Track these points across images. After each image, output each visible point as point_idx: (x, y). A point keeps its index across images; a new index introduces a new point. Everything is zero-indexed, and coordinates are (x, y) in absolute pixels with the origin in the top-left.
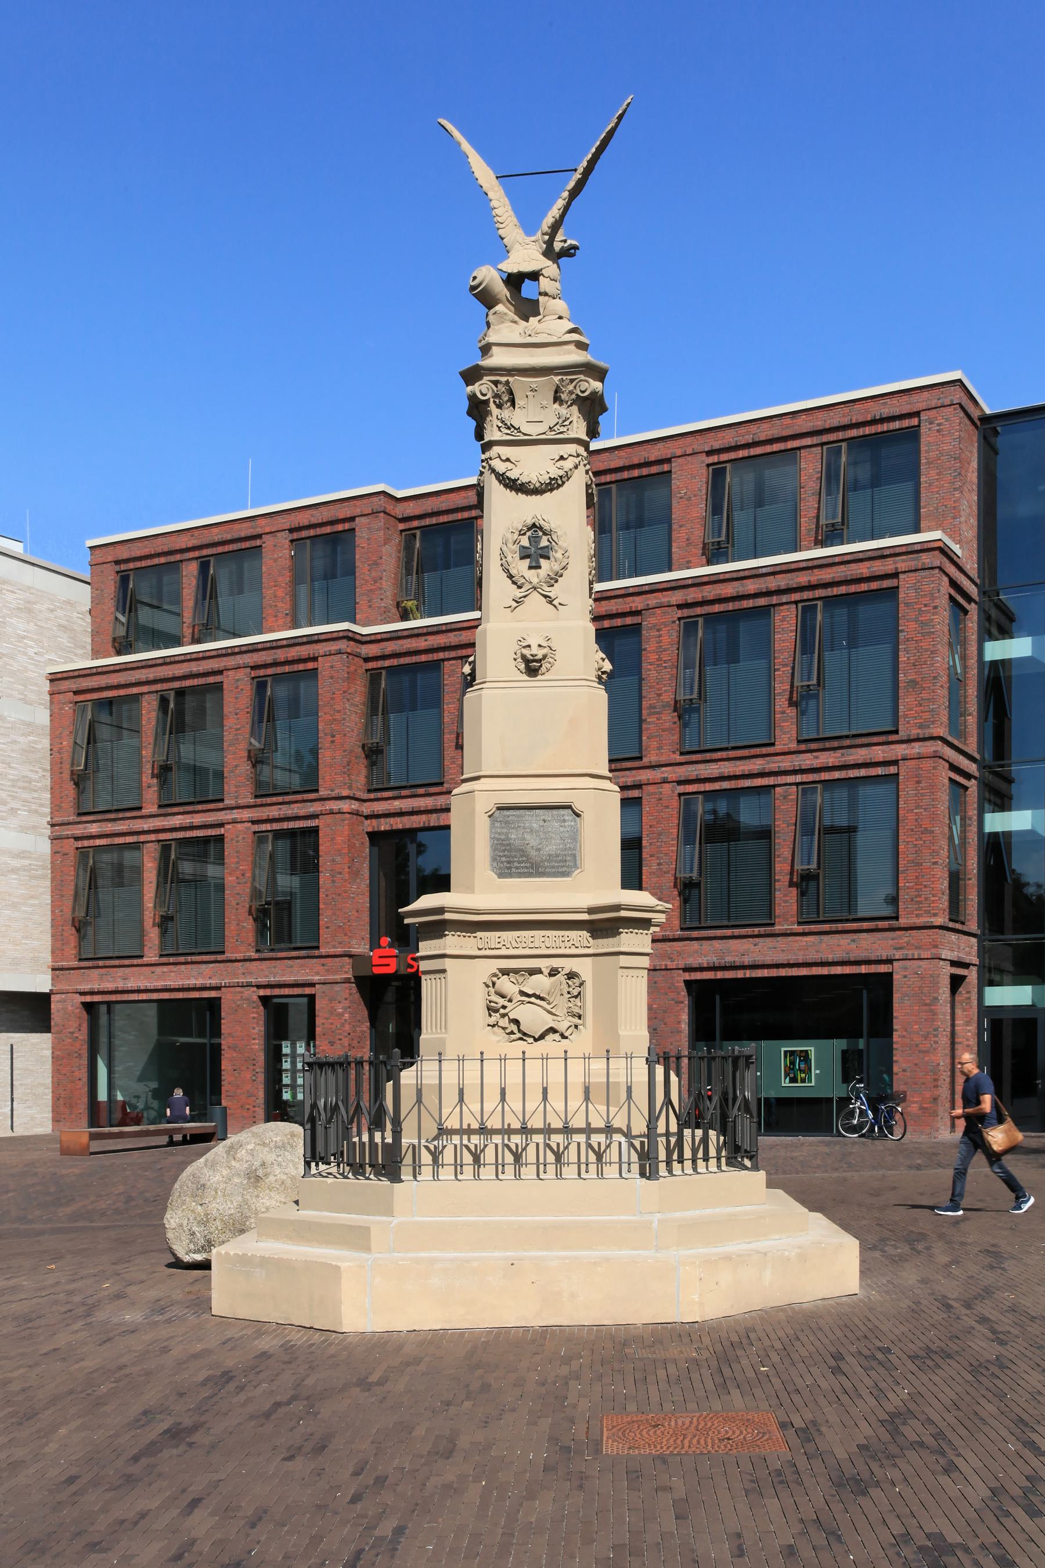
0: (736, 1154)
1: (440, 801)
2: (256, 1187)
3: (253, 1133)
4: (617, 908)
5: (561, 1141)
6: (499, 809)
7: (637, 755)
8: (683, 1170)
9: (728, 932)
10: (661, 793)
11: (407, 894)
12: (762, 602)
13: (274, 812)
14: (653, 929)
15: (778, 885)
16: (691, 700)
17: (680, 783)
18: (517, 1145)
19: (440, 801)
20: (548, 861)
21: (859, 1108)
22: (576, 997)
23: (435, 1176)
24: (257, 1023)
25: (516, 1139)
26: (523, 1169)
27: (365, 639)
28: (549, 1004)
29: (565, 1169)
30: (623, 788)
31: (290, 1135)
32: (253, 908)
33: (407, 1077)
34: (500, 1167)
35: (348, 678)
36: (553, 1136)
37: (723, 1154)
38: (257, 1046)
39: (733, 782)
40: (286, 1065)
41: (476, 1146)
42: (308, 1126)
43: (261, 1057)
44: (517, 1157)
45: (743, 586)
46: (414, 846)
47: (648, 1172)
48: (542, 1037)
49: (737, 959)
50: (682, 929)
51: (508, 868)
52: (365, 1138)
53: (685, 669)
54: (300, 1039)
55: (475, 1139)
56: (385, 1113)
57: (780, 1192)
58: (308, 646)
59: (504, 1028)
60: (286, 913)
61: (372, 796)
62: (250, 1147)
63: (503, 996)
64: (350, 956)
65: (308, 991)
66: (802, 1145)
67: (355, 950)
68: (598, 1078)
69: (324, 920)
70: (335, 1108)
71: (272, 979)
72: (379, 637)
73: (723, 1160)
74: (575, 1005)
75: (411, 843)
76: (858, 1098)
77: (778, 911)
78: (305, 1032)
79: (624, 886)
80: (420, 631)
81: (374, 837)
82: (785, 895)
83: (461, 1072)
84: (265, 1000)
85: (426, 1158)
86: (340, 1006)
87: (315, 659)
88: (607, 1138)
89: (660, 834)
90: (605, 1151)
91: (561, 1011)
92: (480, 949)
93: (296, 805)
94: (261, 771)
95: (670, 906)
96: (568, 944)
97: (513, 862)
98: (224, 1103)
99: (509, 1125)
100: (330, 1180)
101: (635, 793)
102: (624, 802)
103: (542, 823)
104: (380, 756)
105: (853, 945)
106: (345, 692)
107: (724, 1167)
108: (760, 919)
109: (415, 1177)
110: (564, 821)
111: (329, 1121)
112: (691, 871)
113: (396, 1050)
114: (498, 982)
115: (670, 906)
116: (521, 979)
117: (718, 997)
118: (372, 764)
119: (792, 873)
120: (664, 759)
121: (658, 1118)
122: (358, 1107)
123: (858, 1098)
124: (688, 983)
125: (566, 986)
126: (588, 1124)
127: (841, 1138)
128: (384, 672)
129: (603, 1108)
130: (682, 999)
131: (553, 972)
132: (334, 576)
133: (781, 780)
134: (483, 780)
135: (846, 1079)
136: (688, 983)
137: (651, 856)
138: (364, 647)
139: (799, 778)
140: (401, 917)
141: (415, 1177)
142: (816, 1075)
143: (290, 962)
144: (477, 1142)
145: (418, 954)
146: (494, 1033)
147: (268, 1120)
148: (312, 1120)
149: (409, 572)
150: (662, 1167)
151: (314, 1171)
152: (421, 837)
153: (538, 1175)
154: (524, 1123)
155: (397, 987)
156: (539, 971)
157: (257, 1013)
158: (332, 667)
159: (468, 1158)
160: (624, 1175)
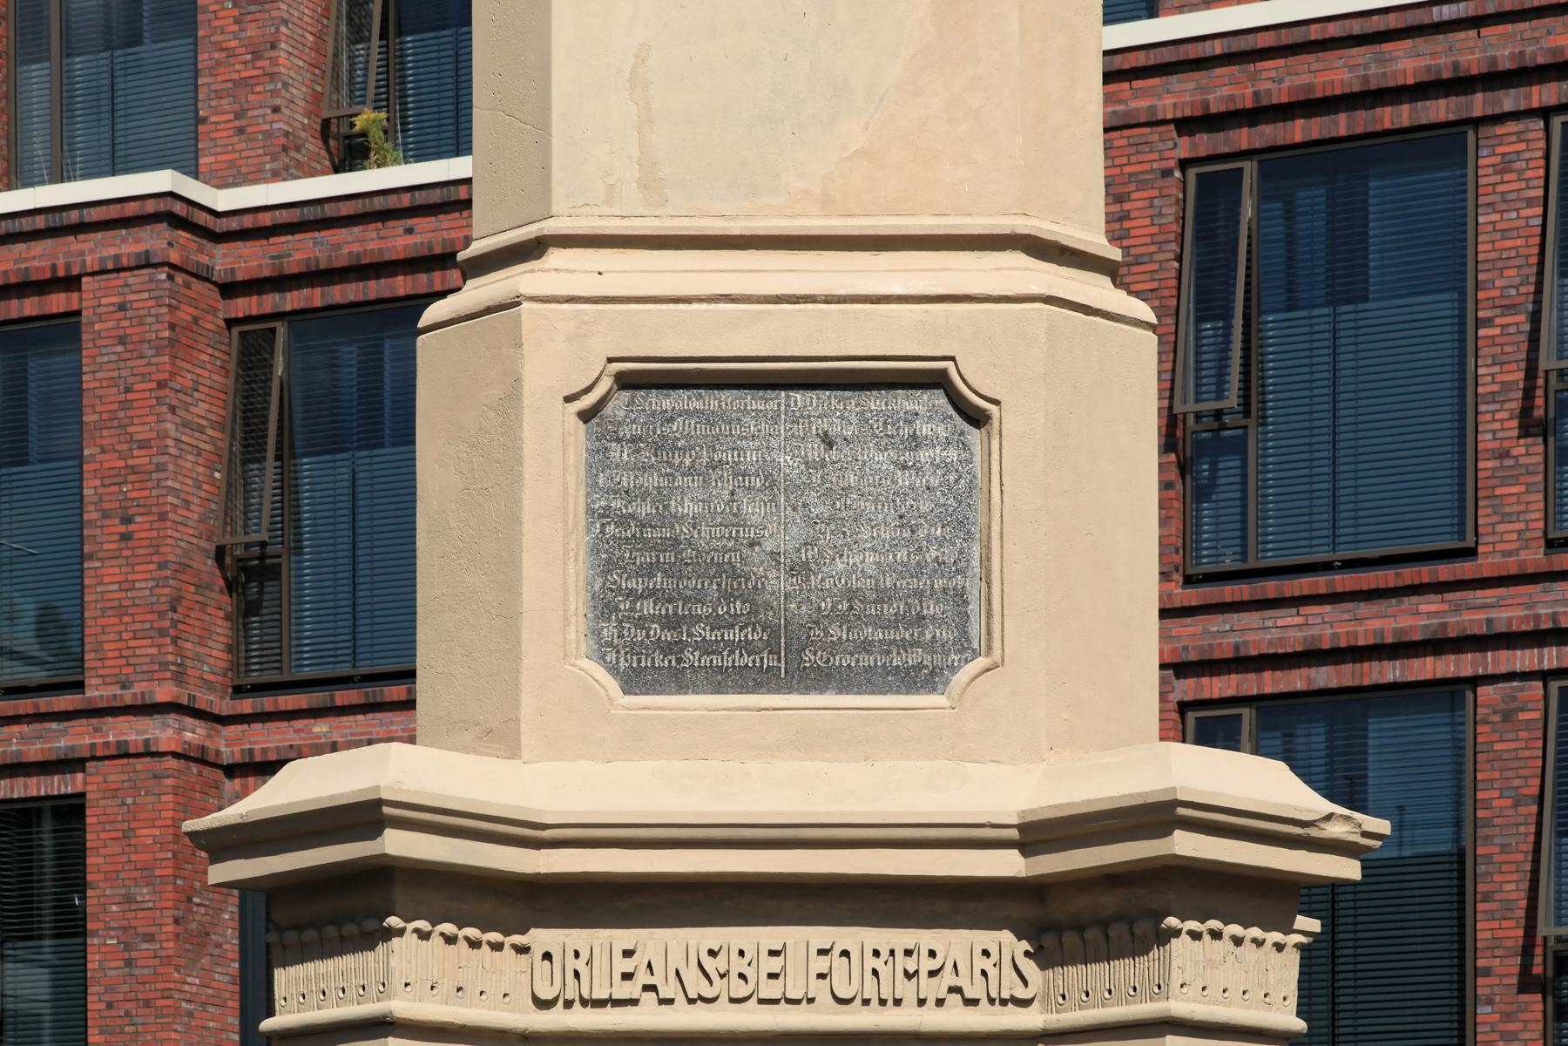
4: (1159, 816)
6: (626, 382)
12: (1439, 110)
15: (1484, 986)
16: (1218, 414)
20: (843, 619)
27: (222, 225)
35: (172, 342)
39: (1347, 668)
45: (1381, 61)
51: (667, 649)
53: (1200, 319)
58: (49, 243)
61: (247, 705)
72: (266, 219)
80: (393, 202)
82: (1507, 1017)
87: (70, 282)
92: (543, 1004)
93: (15, 729)
96: (938, 988)
97: (684, 619)
103: (815, 450)
104: (270, 587)
106: (161, 385)
110: (915, 442)
118: (248, 610)
119: (1527, 950)
128: (281, 329)
132: (134, 39)
133: (1494, 661)
138: (220, 250)
149: (358, 33)
158: (122, 307)
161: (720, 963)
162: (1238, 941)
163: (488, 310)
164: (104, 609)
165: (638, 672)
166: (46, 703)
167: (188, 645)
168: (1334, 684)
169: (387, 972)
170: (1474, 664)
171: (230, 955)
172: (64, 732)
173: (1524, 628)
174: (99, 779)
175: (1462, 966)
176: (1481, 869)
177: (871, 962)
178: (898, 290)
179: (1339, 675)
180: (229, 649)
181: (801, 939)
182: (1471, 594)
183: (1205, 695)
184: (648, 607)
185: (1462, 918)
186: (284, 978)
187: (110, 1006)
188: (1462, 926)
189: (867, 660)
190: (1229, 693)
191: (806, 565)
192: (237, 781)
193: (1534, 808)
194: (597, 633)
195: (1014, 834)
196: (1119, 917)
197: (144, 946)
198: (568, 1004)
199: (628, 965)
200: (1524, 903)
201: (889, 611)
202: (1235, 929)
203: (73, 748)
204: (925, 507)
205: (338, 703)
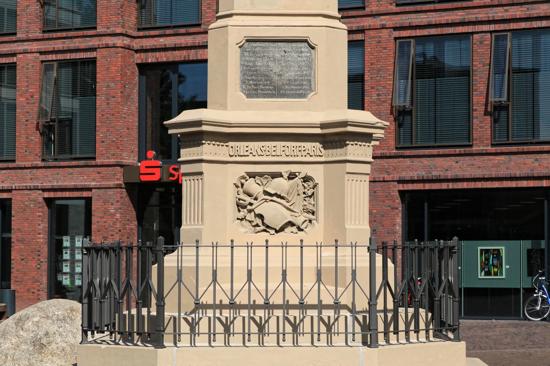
0: (441, 328)
1: (198, 39)
2: (40, 353)
3: (38, 308)
4: (345, 124)
5: (297, 315)
6: (248, 41)
7: (361, 5)
8: (398, 340)
9: (435, 151)
10: (380, 37)
11: (169, 108)
13: (59, 45)
14: (373, 143)
15: (475, 114)
17: (395, 29)
18: (261, 318)
19: (198, 39)
20: (288, 85)
21: (542, 297)
22: (310, 197)
23: (193, 343)
24: (42, 221)
25: (260, 313)
26: (266, 338)
28: (288, 202)
29: (300, 338)
30: (350, 32)
31: (71, 309)
32: (40, 124)
33: (170, 260)
34: (247, 336)
36: (291, 311)
37: (431, 327)
38: (42, 239)
39: (439, 29)
40: (66, 256)
41: (227, 318)
42: (85, 301)
43: (45, 250)
44: (261, 328)
46: (176, 75)
47: (369, 341)
48: (282, 229)
49: (441, 174)
50: (397, 148)
51: (255, 90)
52: (134, 311)
54: (78, 234)
55: (226, 313)
56: (151, 290)
57: (477, 360)
59: (250, 222)
60: (67, 129)
61: (141, 34)
62: (36, 319)
63: (250, 195)
64: (122, 166)
65: (85, 194)
66: (495, 326)
67: (125, 161)
68: (328, 264)
69: (100, 136)
70: (109, 286)
71: (55, 184)
73: (431, 332)
74: (310, 204)
75: (174, 73)
76: (541, 288)
77: (476, 134)
78: (82, 228)
79: (351, 106)
81: (143, 67)
83: (215, 257)
84: (49, 202)
85: (185, 328)
86: (113, 207)
88: (335, 313)
89: (379, 70)
90: (333, 324)
91: (298, 208)
92: (231, 156)
93: (77, 39)
94: (48, 11)
95: (388, 124)
97: (258, 84)
98: (13, 287)
99: (254, 301)
100: (103, 346)
101: (359, 37)
102: (351, 43)
103: (283, 54)
105: (537, 164)
107: (431, 338)
108: (459, 140)
109: (175, 344)
110: (302, 52)
111: (103, 297)
112: (405, 101)
113: (161, 237)
114: (246, 184)
115: (388, 124)
116: (265, 182)
117: (426, 205)
120: (382, 9)
121: (377, 297)
122: (128, 285)
123: (541, 288)
124: (402, 193)
125: (302, 188)
126: (320, 301)
127: (527, 322)
129: (332, 288)
130: (397, 206)
131: (292, 176)
134: (235, 17)
135: (531, 273)
136: (402, 193)
137: (372, 88)
139: (492, 27)
140: (165, 128)
141: (175, 344)
142: (506, 269)
143: (70, 170)
144: (228, 315)
145: (179, 160)
146: (242, 226)
147: (50, 297)
148: (89, 296)
150: (381, 336)
151: (90, 338)
152: (181, 68)
153: (278, 343)
154: (267, 299)
155: (160, 192)
156: (280, 175)
157: (42, 212)
159: (220, 328)
160: (349, 344)
161: (264, 149)
162: (360, 145)
163: (222, 27)
164: (102, 8)
165: (250, 94)
166: (86, 33)
167: (126, 17)
168: (435, 33)
169: (202, 151)
170: (472, 29)
171: (136, 101)
172: (91, 41)
173: (485, 19)
174: (100, 54)
175: (469, 109)
176: (474, 83)
177: (293, 149)
178: (298, 25)
179: (437, 31)
180: (137, 18)
181: (280, 144)
182: (471, 10)
183: (401, 36)
184: (251, 82)
185: (469, 96)
186: (182, 151)
187: (102, 115)
188: (469, 98)
189: (292, 92)
190: (408, 35)
191: (281, 75)
192: (138, 54)
193: (488, 67)
194: (242, 87)
195: (319, 125)
196: (338, 141)
197: (112, 99)
198: (236, 156)
199: (247, 149)
200: (485, 92)
201: (296, 83)
202: (360, 143)
203: (93, 45)
204: (303, 64)
205: (167, 33)
